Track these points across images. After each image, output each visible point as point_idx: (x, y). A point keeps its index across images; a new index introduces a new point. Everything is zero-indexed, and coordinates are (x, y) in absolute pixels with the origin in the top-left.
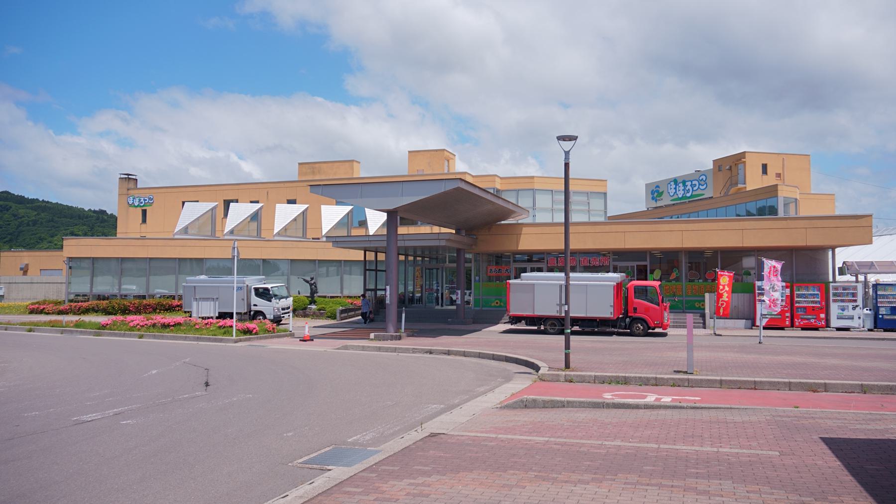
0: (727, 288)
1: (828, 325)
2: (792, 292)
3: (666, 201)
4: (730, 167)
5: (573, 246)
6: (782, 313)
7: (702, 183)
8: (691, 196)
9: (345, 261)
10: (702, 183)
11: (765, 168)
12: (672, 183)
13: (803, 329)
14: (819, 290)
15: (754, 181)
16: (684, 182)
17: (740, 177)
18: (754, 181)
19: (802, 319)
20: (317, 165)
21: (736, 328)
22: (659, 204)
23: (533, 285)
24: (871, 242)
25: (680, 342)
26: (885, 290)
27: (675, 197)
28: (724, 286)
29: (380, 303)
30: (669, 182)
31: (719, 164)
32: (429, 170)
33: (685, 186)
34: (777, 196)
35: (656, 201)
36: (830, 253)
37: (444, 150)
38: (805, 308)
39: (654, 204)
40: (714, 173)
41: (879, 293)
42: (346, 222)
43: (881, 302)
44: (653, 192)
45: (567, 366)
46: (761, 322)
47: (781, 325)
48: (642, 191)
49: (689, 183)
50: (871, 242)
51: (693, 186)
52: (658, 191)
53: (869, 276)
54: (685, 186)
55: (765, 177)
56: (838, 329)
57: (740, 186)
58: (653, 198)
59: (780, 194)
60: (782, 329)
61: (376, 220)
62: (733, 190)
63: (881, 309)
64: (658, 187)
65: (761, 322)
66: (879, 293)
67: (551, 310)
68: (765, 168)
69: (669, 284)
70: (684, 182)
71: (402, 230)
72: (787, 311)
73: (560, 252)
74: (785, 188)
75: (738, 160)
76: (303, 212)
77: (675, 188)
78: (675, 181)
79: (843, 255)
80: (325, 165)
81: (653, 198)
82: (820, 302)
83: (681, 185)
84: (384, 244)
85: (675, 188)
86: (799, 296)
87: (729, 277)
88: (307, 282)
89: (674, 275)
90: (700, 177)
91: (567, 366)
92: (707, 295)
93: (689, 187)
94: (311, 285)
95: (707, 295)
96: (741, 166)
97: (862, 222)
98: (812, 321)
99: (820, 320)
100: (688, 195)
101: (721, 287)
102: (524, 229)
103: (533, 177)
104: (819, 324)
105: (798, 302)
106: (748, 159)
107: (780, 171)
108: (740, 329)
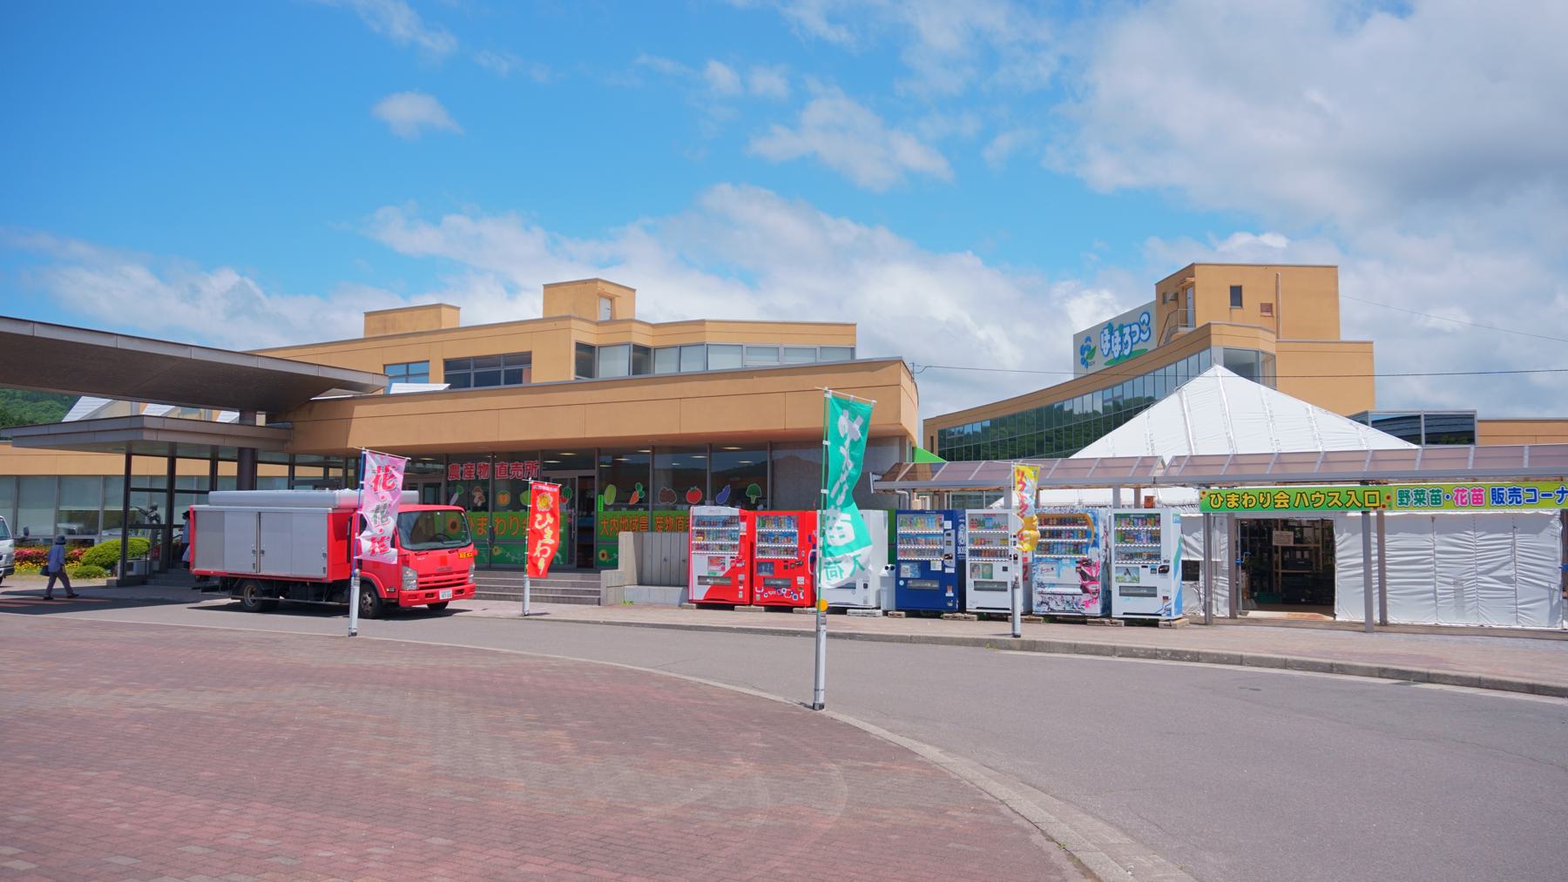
0: (550, 520)
1: (813, 600)
2: (751, 529)
3: (1099, 364)
6: (734, 571)
10: (1144, 328)
11: (1236, 294)
13: (772, 608)
14: (798, 525)
19: (769, 587)
20: (390, 316)
21: (663, 607)
22: (1092, 370)
23: (223, 512)
25: (495, 626)
26: (911, 524)
28: (544, 513)
37: (596, 280)
38: (772, 562)
39: (1084, 371)
41: (901, 530)
43: (905, 552)
47: (729, 600)
48: (1068, 348)
49: (1126, 330)
51: (1132, 334)
55: (1236, 311)
56: (1131, 622)
59: (1214, 340)
60: (730, 607)
63: (904, 567)
66: (901, 530)
67: (313, 564)
68: (1236, 294)
69: (632, 513)
72: (740, 570)
80: (399, 315)
82: (799, 550)
86: (765, 537)
87: (553, 494)
89: (638, 494)
93: (1127, 338)
97: (882, 376)
98: (784, 591)
99: (794, 587)
101: (539, 517)
102: (357, 408)
103: (702, 322)
104: (795, 598)
105: (762, 551)
106: (1199, 279)
107: (1271, 300)
108: (666, 606)
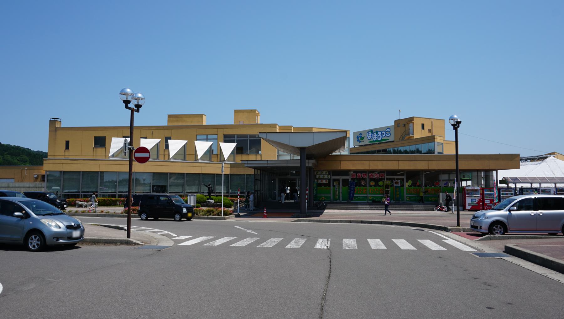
3: (366, 142)
4: (404, 125)
8: (381, 140)
9: (187, 174)
15: (418, 134)
16: (377, 132)
17: (411, 131)
18: (418, 134)
22: (362, 144)
24: (519, 168)
27: (372, 140)
30: (367, 132)
31: (398, 123)
32: (244, 120)
33: (377, 134)
34: (434, 142)
36: (494, 172)
39: (358, 144)
40: (395, 128)
42: (210, 152)
44: (358, 137)
45: (458, 225)
46: (468, 207)
49: (380, 133)
50: (519, 168)
52: (361, 137)
53: (517, 184)
54: (377, 134)
57: (411, 135)
58: (358, 141)
61: (227, 148)
62: (407, 137)
64: (361, 134)
65: (468, 207)
70: (377, 132)
74: (438, 137)
75: (410, 120)
76: (157, 144)
78: (372, 131)
79: (502, 174)
81: (358, 141)
83: (375, 134)
84: (299, 165)
86: (503, 194)
88: (207, 186)
90: (387, 130)
91: (458, 225)
92: (441, 194)
93: (380, 135)
94: (209, 188)
95: (441, 194)
96: (411, 125)
100: (379, 139)
106: (415, 121)
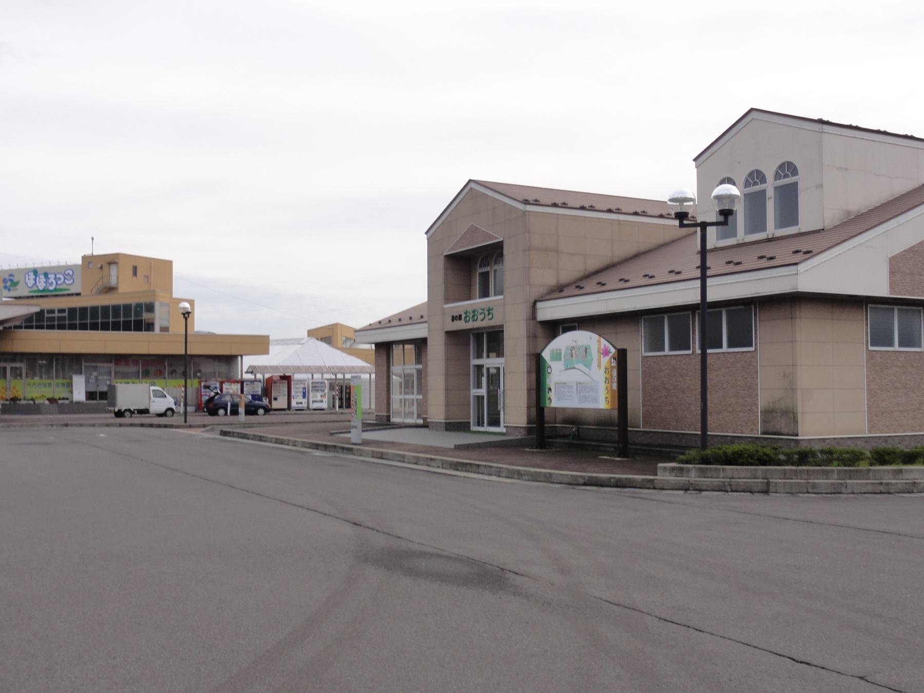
5: (189, 353)
7: (69, 277)
8: (55, 290)
11: (135, 270)
12: (32, 274)
16: (46, 275)
27: (35, 288)
29: (15, 284)
30: (26, 271)
35: (9, 290)
49: (52, 277)
52: (11, 281)
55: (134, 278)
63: (561, 398)
64: (11, 275)
68: (135, 270)
70: (46, 275)
71: (709, 351)
73: (603, 422)
77: (35, 280)
78: (35, 272)
83: (42, 277)
85: (35, 280)
100: (51, 288)
